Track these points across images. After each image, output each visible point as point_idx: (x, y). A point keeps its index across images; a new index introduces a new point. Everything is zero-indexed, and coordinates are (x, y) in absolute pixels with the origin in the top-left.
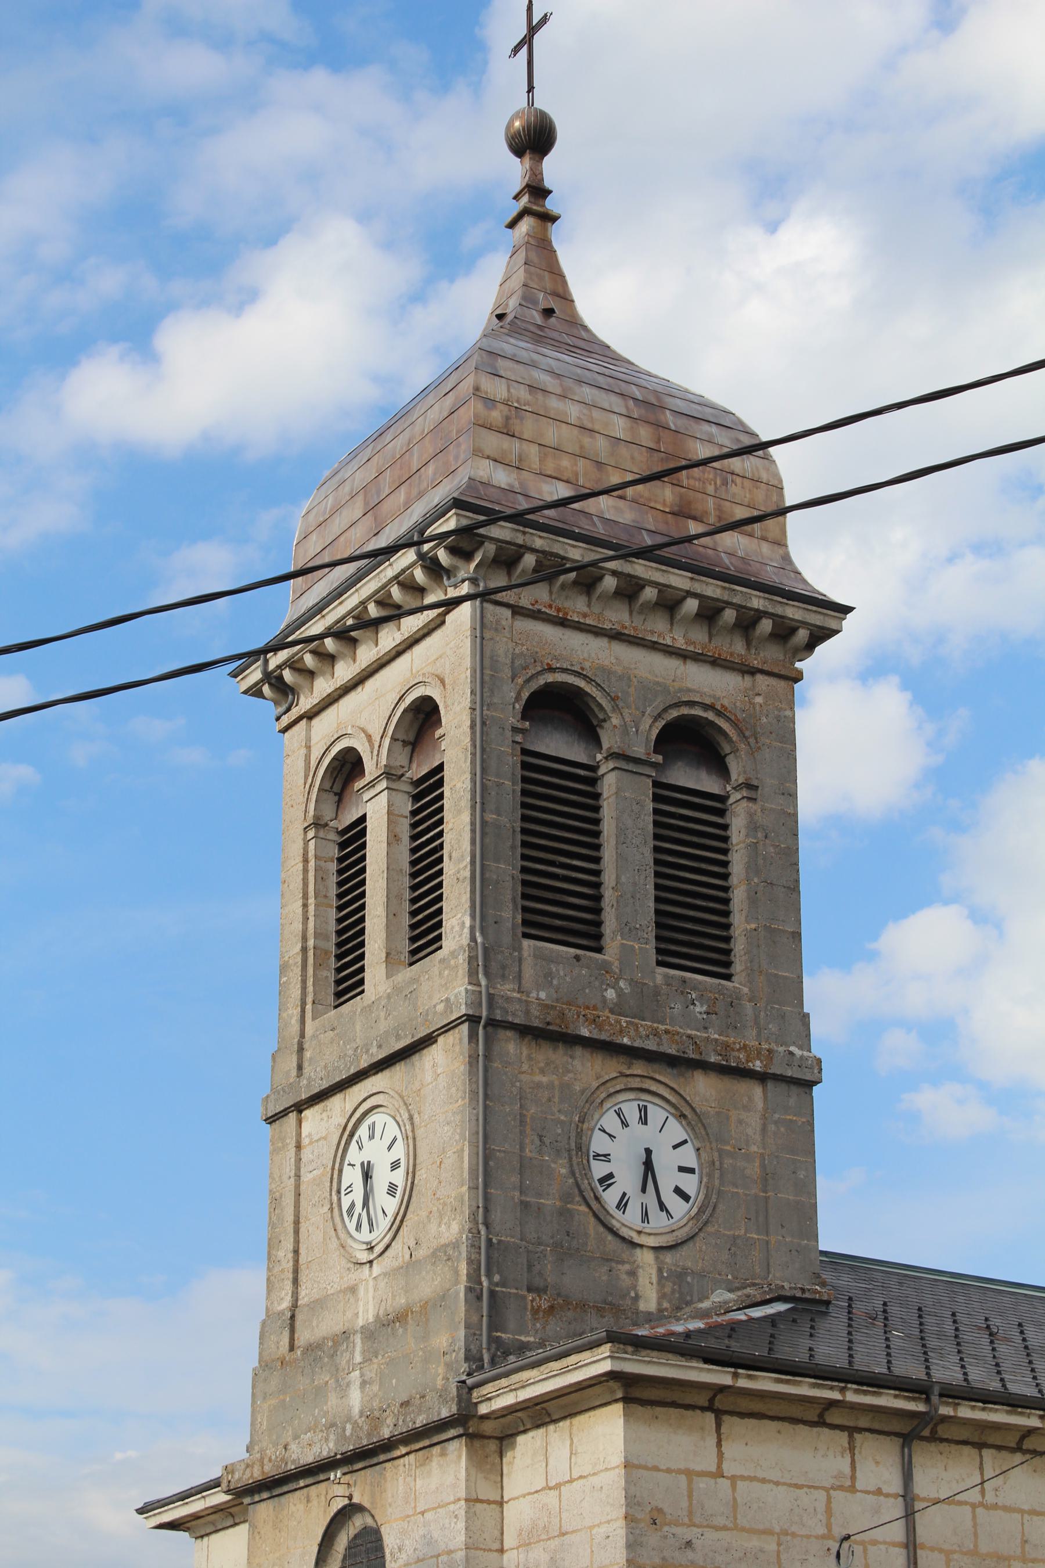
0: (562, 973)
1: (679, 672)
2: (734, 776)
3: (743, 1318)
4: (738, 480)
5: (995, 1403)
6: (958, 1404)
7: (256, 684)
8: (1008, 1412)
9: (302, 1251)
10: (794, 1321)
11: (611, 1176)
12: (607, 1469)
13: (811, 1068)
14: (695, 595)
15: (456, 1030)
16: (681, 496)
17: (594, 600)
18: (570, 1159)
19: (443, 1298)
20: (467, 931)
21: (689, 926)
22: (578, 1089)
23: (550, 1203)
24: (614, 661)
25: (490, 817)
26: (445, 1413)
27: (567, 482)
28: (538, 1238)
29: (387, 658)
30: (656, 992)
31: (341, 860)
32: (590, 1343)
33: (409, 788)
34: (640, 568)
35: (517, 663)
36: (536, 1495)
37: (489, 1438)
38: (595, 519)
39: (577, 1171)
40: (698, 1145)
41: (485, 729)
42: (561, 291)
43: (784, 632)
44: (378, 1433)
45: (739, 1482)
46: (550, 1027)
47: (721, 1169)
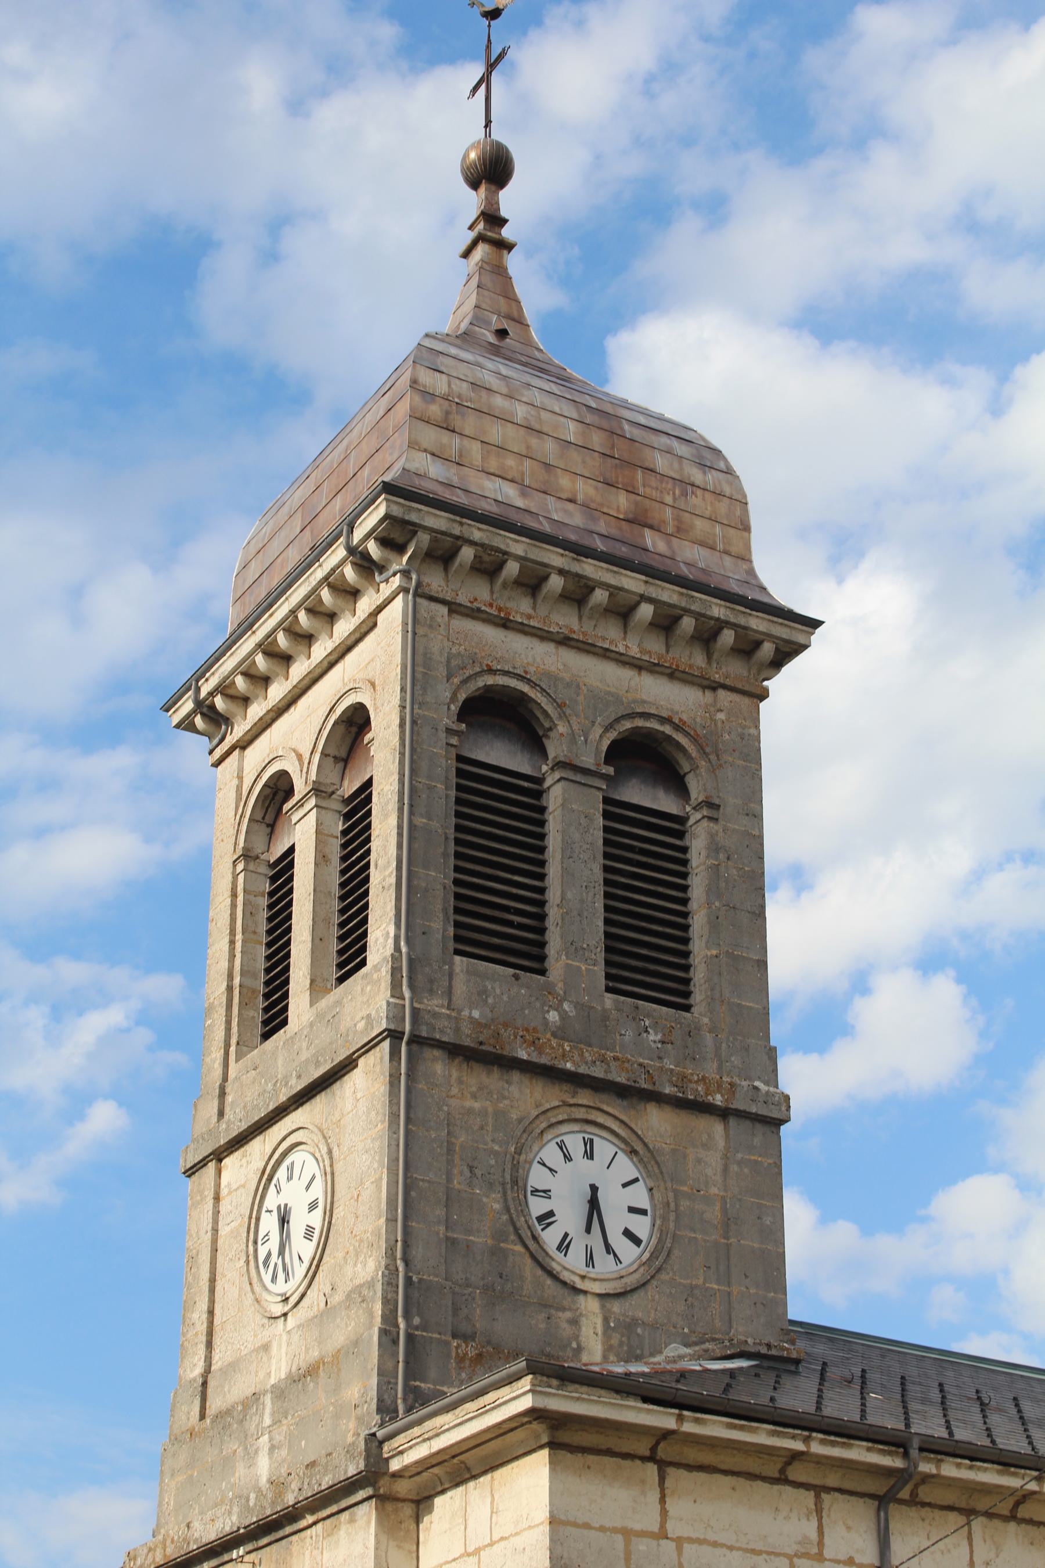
0: (498, 991)
1: (633, 683)
2: (694, 794)
3: (698, 1368)
4: (699, 492)
5: (984, 1461)
6: (942, 1461)
7: (188, 716)
8: (999, 1472)
9: (217, 1311)
10: (757, 1375)
11: (551, 1214)
12: (530, 1527)
13: (779, 1104)
14: (650, 600)
15: (378, 1049)
16: (637, 503)
17: (539, 601)
18: (505, 1194)
19: (356, 1343)
20: (391, 941)
21: (644, 952)
22: (515, 1117)
23: (481, 1240)
24: (562, 667)
25: (420, 821)
26: (352, 1471)
27: (512, 481)
28: (467, 1279)
29: (319, 671)
30: (605, 1017)
31: (271, 894)
32: (509, 1376)
33: (338, 806)
34: (589, 568)
35: (454, 663)
36: (454, 1563)
37: (404, 1500)
38: (541, 518)
39: (512, 1207)
40: (651, 1184)
41: (416, 728)
42: (515, 314)
43: (747, 647)
44: (283, 1500)
45: (685, 1545)
46: (483, 1048)
47: (676, 1210)
